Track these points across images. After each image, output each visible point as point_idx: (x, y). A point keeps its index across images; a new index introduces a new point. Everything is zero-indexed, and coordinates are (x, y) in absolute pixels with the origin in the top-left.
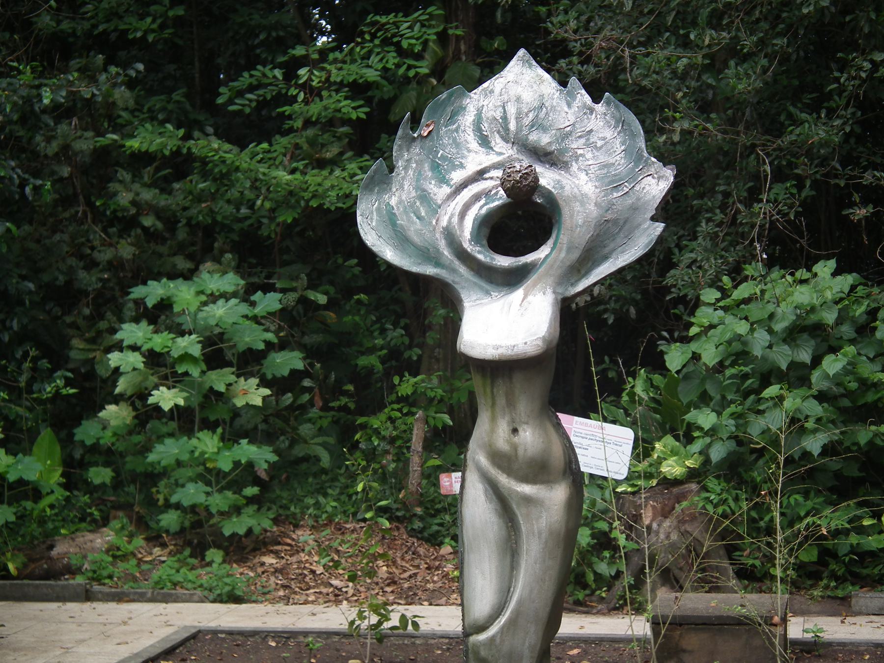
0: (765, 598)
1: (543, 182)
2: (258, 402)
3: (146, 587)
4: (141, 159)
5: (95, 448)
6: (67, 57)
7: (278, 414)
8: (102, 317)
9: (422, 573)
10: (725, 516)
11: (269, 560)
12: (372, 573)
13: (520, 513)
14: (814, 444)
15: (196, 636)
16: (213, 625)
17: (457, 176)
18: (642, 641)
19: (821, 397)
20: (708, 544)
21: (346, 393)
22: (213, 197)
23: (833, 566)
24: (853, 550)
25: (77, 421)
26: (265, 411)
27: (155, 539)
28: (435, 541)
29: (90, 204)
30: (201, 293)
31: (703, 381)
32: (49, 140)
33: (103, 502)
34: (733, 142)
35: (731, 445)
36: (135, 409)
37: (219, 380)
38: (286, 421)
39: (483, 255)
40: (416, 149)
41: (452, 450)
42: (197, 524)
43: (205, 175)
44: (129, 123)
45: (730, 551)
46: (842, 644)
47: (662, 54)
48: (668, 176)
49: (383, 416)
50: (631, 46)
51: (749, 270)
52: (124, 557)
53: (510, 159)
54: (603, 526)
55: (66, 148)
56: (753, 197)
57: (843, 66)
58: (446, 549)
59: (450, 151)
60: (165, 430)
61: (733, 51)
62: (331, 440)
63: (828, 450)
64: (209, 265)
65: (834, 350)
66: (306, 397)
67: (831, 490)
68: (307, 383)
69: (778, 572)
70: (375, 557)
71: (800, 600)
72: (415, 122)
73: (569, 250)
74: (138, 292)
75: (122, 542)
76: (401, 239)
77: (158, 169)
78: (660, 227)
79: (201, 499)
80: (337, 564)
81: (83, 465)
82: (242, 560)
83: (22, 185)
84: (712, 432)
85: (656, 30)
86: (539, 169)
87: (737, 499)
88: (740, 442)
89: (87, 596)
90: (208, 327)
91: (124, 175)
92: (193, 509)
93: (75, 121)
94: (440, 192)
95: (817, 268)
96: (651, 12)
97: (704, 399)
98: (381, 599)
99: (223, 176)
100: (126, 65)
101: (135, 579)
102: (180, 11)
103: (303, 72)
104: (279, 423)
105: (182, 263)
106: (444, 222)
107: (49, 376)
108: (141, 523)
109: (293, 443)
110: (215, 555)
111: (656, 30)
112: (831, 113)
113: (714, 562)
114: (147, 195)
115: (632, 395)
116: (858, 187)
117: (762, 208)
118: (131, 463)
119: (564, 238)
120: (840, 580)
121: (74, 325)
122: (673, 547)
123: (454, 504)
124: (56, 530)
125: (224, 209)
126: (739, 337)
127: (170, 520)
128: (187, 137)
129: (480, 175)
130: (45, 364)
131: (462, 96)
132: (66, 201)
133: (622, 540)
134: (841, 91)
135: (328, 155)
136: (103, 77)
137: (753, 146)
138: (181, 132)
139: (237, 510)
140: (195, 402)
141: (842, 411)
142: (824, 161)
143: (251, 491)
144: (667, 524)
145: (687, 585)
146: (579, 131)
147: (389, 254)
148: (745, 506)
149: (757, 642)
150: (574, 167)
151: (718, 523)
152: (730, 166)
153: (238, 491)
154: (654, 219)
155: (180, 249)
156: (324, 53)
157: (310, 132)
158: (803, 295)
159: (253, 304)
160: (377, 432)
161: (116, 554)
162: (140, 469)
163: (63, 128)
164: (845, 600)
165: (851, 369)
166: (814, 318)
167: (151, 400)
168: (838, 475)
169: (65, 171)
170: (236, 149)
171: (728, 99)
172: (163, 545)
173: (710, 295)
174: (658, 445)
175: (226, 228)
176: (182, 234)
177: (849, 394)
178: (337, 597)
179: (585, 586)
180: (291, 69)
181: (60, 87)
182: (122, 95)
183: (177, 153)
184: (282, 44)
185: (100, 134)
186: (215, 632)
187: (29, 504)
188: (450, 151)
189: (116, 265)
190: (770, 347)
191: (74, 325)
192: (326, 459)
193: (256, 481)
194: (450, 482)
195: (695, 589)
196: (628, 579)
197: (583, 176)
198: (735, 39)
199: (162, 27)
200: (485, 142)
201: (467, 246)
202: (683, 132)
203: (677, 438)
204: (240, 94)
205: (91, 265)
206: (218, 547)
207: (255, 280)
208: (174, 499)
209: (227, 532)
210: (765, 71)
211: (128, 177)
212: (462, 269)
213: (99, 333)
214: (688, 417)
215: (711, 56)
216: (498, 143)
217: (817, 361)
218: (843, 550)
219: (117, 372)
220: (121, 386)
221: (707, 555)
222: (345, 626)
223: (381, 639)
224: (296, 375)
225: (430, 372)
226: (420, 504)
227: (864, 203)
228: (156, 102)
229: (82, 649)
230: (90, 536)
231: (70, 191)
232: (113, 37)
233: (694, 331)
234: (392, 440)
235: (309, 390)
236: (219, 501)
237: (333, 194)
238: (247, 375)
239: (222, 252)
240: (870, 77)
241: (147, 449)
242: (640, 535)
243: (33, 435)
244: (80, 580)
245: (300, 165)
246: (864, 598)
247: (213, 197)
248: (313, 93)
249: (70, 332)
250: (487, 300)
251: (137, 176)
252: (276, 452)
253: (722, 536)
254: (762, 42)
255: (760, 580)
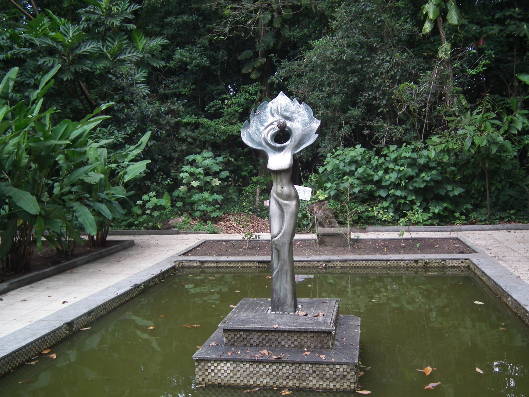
0: (345, 228)
1: (288, 125)
2: (218, 184)
3: (192, 231)
4: (187, 124)
5: (178, 197)
6: (167, 99)
7: (223, 187)
8: (179, 164)
9: (260, 225)
10: (335, 209)
11: (222, 223)
12: (248, 225)
13: (284, 208)
14: (356, 190)
15: (205, 242)
16: (209, 239)
17: (266, 124)
18: (315, 240)
19: (358, 179)
20: (330, 216)
21: (240, 181)
22: (205, 133)
23: (362, 220)
24: (367, 216)
25: (173, 190)
26: (220, 187)
27: (194, 219)
28: (263, 217)
29: (174, 135)
30: (202, 157)
31: (328, 175)
32: (164, 120)
33: (181, 210)
34: (334, 115)
35: (336, 191)
36: (188, 187)
37: (208, 179)
38: (226, 189)
39: (273, 144)
40: (255, 118)
41: (267, 195)
42: (204, 215)
43: (203, 128)
44: (183, 115)
45: (336, 217)
46: (364, 239)
47: (316, 94)
48: (319, 122)
49: (249, 187)
50: (308, 92)
51: (338, 148)
52: (187, 223)
53: (279, 119)
54: (305, 212)
55: (168, 122)
56: (340, 129)
57: (361, 96)
58: (266, 219)
59: (264, 118)
60: (195, 192)
61: (334, 93)
62: (237, 194)
63: (360, 192)
64: (205, 150)
65: (360, 167)
66: (230, 183)
67: (361, 202)
68: (230, 179)
69: (348, 222)
70: (248, 222)
71: (354, 229)
72: (255, 112)
73: (295, 142)
74: (187, 158)
75: (186, 219)
76: (253, 141)
77: (191, 127)
78: (317, 135)
79: (205, 208)
80: (239, 223)
81: (176, 201)
82: (216, 223)
83: (157, 132)
84: (330, 188)
85: (315, 88)
86: (287, 122)
87: (337, 205)
88: (338, 190)
89: (178, 233)
90: (205, 166)
91: (183, 128)
92: (203, 211)
93: (170, 115)
94: (262, 128)
95: (356, 147)
96: (313, 83)
97: (329, 180)
98: (250, 232)
99: (208, 128)
100: (182, 101)
101: (190, 229)
102: (194, 87)
103: (226, 101)
104: (223, 189)
105: (198, 150)
106: (263, 136)
107: (166, 179)
108: (191, 215)
109: (227, 194)
110: (209, 222)
111: (315, 88)
112: (359, 107)
113: (332, 220)
114: (189, 133)
115: (311, 179)
116: (366, 126)
117: (342, 132)
118: (188, 200)
119: (293, 139)
120: (363, 224)
121: (172, 166)
122: (322, 217)
123: (267, 209)
124: (170, 217)
125: (208, 137)
126: (336, 164)
127: (198, 214)
128: (198, 118)
129: (272, 124)
130: (165, 176)
131: (266, 104)
132: (169, 135)
133: (309, 216)
134: (361, 102)
135: (233, 122)
136: (177, 104)
137: (339, 117)
138: (196, 117)
139: (214, 211)
140: (203, 185)
141: (363, 182)
142: (357, 120)
143: (217, 206)
144: (320, 211)
145: (326, 226)
146: (296, 112)
147: (250, 144)
148: (339, 206)
149: (343, 239)
150: (295, 121)
151: (333, 210)
152: (334, 122)
153: (214, 207)
154: (316, 133)
155: (198, 146)
156: (231, 97)
157: (229, 116)
158: (353, 153)
159: (216, 160)
160: (248, 191)
161: (185, 223)
162: (190, 202)
163: (167, 117)
164: (365, 229)
165: (365, 171)
166: (355, 159)
167: (191, 185)
168: (362, 198)
169: (168, 128)
170: (210, 121)
171: (333, 105)
172: (196, 220)
173: (329, 155)
174: (318, 192)
175: (208, 142)
176: (198, 143)
177: (365, 178)
178: (240, 232)
179: (300, 227)
180: (223, 100)
181: (166, 107)
182: (181, 108)
183: (196, 123)
184: (220, 94)
185: (176, 118)
186: (210, 241)
187: (163, 211)
188: (264, 118)
189: (182, 151)
190: (344, 166)
191: (172, 166)
192: (236, 199)
193: (219, 204)
194: (266, 203)
195: (328, 227)
196: (311, 225)
197: (297, 123)
198: (334, 89)
199: (190, 91)
200: (273, 115)
201: (269, 141)
202: (322, 114)
203: (322, 190)
204: (211, 107)
205: (175, 151)
206: (210, 220)
207: (217, 154)
208: (198, 209)
209: (212, 217)
210: (342, 97)
211: (184, 129)
212: (268, 147)
213: (178, 168)
214: (324, 185)
215: (328, 94)
216: (276, 115)
217: (356, 170)
218: (364, 216)
219: (183, 178)
220: (184, 181)
221: (330, 218)
222: (242, 238)
223: (251, 241)
224: (228, 177)
225: (260, 175)
226: (259, 208)
227: (367, 130)
228: (189, 109)
229: (177, 246)
230: (178, 218)
231: (169, 133)
232: (177, 93)
233: (325, 163)
234: (252, 193)
235: (230, 181)
236: (210, 209)
237: (235, 131)
238: (215, 178)
239: (208, 147)
240: (368, 98)
241: (191, 197)
242: (314, 214)
243: (163, 194)
244: (176, 229)
245: (226, 124)
246: (369, 228)
247: (205, 133)
248: (229, 106)
249: (171, 168)
250: (274, 155)
251: (186, 129)
252: (223, 197)
253: (334, 214)
254: (341, 91)
255: (344, 224)
